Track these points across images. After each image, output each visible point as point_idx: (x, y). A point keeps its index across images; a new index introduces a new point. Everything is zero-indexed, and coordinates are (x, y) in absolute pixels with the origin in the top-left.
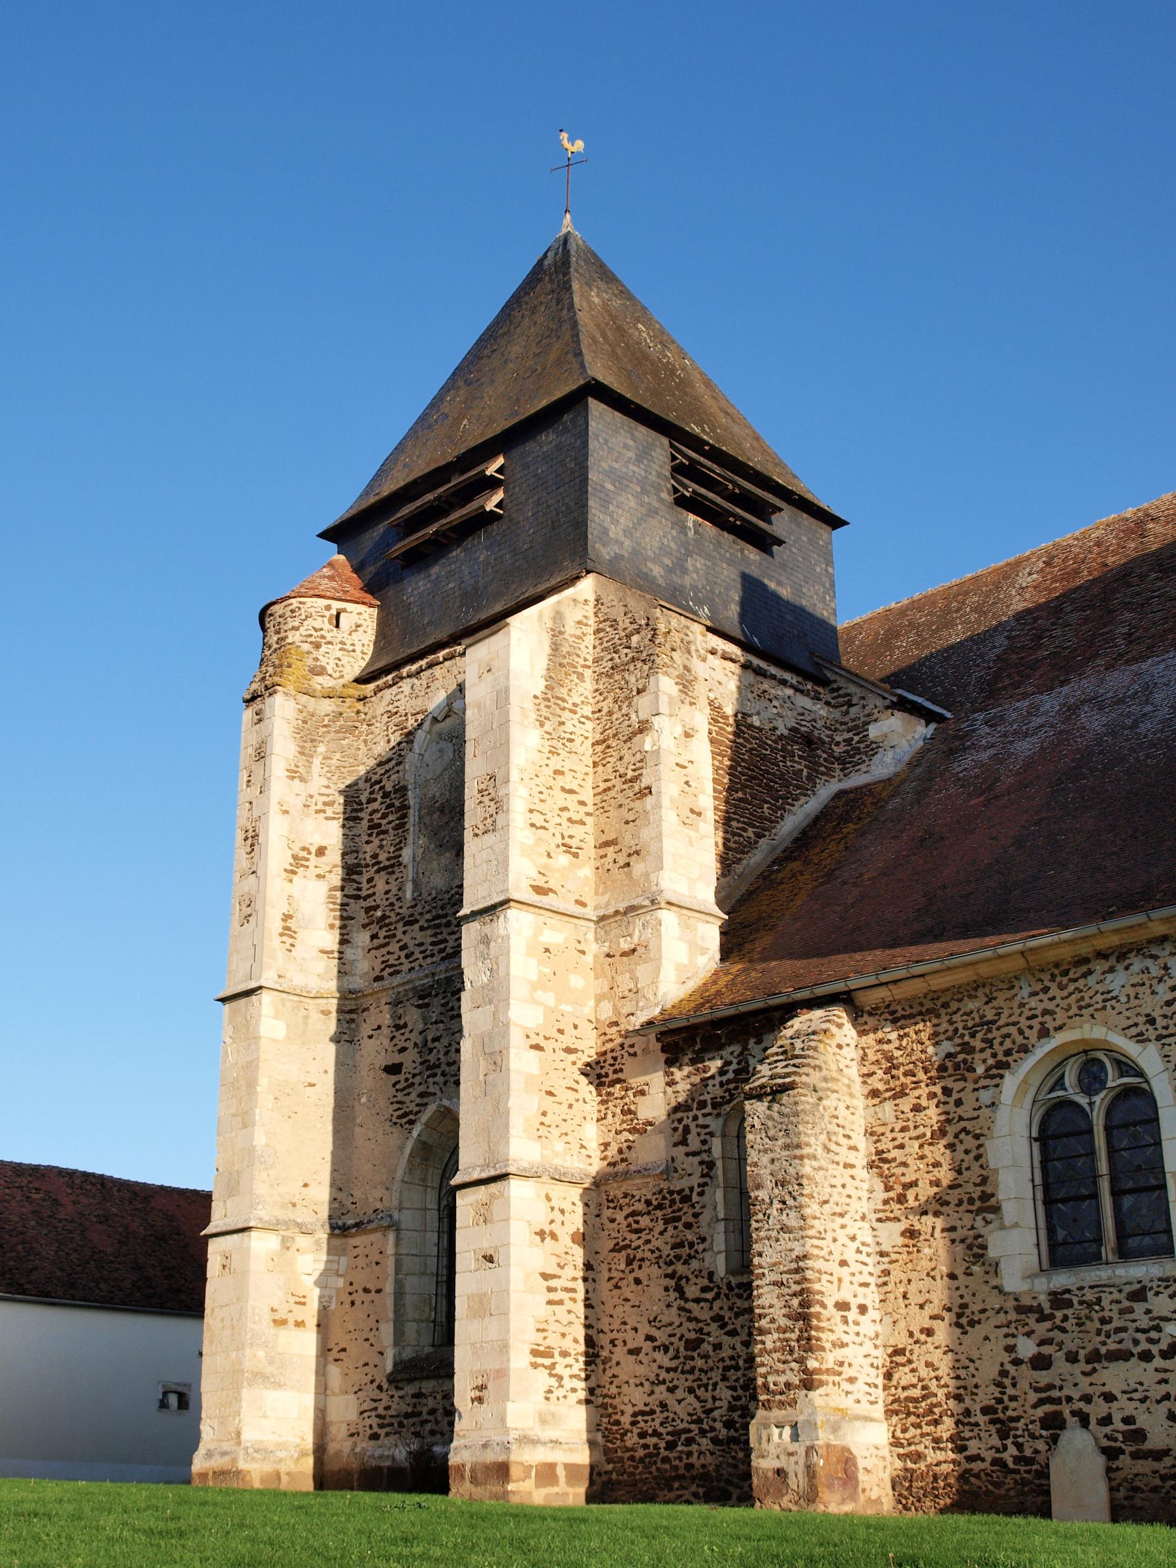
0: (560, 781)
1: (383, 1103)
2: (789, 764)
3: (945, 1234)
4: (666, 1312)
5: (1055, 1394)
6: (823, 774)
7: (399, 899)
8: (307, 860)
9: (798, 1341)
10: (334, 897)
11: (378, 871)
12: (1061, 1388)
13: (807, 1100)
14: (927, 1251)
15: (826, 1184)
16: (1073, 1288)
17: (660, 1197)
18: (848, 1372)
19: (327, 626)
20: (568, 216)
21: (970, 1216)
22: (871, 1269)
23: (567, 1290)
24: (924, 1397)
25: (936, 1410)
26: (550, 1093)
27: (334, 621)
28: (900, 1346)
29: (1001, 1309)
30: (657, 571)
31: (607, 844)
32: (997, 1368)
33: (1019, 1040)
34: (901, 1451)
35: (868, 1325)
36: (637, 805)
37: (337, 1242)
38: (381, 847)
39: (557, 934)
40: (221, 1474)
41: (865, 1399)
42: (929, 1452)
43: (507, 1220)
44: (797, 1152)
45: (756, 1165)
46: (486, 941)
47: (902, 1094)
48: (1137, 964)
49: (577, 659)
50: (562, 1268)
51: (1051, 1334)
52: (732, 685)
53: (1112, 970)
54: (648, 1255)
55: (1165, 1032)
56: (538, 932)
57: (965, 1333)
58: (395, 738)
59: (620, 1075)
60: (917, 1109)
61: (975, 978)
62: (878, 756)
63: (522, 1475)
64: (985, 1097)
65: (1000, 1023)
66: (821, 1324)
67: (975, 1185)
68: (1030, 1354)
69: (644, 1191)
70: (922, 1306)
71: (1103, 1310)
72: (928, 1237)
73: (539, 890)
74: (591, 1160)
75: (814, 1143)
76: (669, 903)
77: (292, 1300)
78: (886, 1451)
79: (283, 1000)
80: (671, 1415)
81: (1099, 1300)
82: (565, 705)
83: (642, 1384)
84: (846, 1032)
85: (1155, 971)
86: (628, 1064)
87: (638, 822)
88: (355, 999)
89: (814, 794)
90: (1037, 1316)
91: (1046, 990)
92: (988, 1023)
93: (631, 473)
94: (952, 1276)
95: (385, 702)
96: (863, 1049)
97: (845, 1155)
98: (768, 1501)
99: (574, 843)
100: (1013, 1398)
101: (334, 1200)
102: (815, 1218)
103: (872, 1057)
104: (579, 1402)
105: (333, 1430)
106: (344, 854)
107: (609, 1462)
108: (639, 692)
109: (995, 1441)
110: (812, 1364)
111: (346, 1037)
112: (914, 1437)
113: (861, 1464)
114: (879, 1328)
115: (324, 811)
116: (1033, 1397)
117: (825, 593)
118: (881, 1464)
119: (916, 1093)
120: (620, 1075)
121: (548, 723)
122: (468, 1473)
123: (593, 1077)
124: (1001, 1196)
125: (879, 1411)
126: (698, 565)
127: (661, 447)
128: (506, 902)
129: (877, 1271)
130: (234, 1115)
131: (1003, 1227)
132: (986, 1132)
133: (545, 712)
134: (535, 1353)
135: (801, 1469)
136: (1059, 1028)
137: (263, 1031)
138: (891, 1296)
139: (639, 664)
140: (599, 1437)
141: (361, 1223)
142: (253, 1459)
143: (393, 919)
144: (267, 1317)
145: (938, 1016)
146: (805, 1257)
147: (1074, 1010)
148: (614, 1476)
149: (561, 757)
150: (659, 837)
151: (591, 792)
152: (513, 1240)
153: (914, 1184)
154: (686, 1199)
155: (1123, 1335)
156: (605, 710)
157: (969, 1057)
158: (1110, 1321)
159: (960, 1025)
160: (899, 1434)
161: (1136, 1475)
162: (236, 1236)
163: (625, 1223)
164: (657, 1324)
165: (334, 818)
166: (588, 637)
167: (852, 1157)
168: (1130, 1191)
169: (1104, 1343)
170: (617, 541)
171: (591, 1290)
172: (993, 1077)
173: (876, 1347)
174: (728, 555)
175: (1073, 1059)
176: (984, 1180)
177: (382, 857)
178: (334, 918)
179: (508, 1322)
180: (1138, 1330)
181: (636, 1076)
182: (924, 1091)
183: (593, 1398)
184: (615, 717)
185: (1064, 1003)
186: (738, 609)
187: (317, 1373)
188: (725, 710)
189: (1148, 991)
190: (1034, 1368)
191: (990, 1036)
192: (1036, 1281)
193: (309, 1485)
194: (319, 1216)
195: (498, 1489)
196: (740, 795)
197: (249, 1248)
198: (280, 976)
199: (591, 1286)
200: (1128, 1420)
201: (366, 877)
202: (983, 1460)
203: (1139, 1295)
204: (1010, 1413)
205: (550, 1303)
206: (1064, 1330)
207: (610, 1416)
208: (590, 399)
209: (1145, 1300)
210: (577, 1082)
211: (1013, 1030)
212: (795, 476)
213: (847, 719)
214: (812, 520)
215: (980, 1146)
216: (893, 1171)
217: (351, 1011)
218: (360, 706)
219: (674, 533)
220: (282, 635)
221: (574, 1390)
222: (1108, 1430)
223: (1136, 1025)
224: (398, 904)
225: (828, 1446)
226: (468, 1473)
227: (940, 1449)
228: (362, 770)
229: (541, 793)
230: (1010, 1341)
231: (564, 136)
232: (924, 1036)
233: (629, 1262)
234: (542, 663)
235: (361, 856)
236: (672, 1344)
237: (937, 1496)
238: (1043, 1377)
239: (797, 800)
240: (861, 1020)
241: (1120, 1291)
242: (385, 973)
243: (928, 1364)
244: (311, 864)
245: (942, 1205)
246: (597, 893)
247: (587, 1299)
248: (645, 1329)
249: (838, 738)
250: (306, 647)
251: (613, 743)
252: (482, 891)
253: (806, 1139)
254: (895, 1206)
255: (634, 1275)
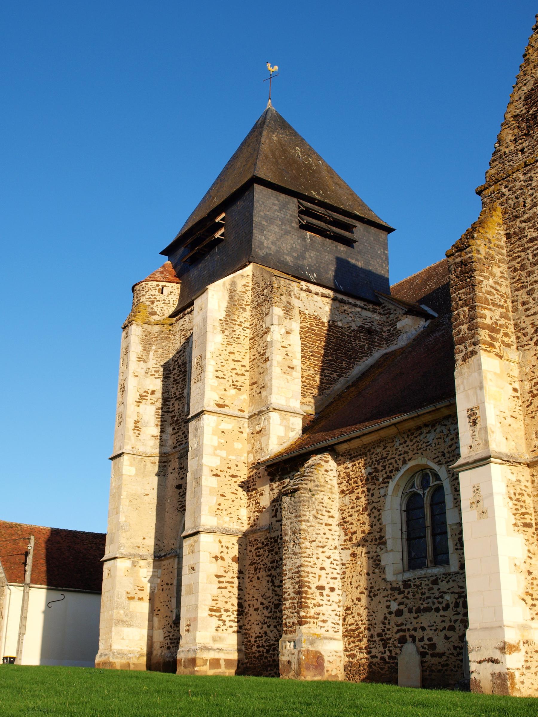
0: (232, 357)
1: (175, 502)
2: (357, 342)
3: (366, 555)
4: (268, 592)
5: (403, 627)
6: (376, 346)
7: (182, 412)
8: (147, 396)
9: (297, 603)
10: (158, 412)
11: (176, 400)
12: (406, 625)
13: (305, 495)
14: (359, 563)
15: (314, 533)
16: (412, 579)
17: (267, 540)
18: (321, 617)
19: (157, 293)
20: (270, 101)
21: (375, 546)
22: (338, 571)
23: (229, 582)
24: (357, 629)
25: (361, 635)
26: (223, 496)
27: (161, 291)
28: (349, 606)
29: (385, 588)
30: (289, 259)
31: (253, 384)
32: (383, 616)
33: (395, 465)
34: (348, 653)
35: (334, 597)
36: (264, 365)
37: (157, 563)
38: (177, 389)
39: (228, 425)
40: (105, 663)
41: (331, 630)
42: (358, 654)
43: (199, 552)
44: (300, 519)
45: (285, 525)
46: (196, 429)
47: (352, 492)
48: (439, 428)
49: (242, 302)
50: (227, 572)
51: (403, 600)
52: (327, 308)
53: (429, 432)
54: (262, 566)
55: (449, 460)
56: (218, 424)
57: (372, 600)
58: (183, 341)
59: (255, 487)
60: (358, 498)
61: (379, 438)
62: (401, 337)
63: (202, 664)
64: (382, 491)
65: (388, 458)
66: (308, 596)
67: (378, 532)
68: (395, 610)
69: (261, 538)
70: (357, 588)
71: (422, 589)
72: (360, 556)
73: (219, 406)
74: (243, 525)
75: (309, 515)
76: (274, 409)
77: (137, 588)
78: (342, 654)
79: (134, 458)
80: (268, 638)
81: (421, 584)
82: (236, 323)
83: (258, 624)
84: (332, 464)
85: (446, 432)
86: (258, 481)
87: (264, 373)
88: (166, 457)
89: (371, 355)
90: (398, 592)
91: (405, 442)
92: (384, 458)
93: (276, 216)
94: (368, 574)
95: (180, 326)
96: (339, 472)
97: (326, 519)
98: (284, 675)
99: (238, 384)
100: (388, 629)
101: (156, 545)
102: (307, 548)
103: (342, 475)
104: (234, 632)
105: (155, 645)
106: (163, 393)
107: (246, 658)
108: (266, 315)
109: (382, 649)
110: (302, 614)
111: (162, 473)
112: (352, 647)
113: (326, 659)
114: (341, 598)
115: (155, 375)
116: (396, 629)
117: (382, 263)
118: (339, 659)
119: (357, 491)
120: (255, 487)
121: (226, 331)
122: (183, 663)
123: (245, 488)
124: (387, 537)
125: (340, 635)
126: (312, 255)
127: (293, 204)
128: (202, 412)
129: (341, 572)
130: (114, 509)
131: (387, 552)
132: (382, 508)
133: (225, 326)
134: (211, 610)
135: (296, 661)
136: (410, 460)
137: (124, 472)
138: (346, 583)
139: (266, 302)
140: (243, 648)
141: (166, 554)
142: (117, 657)
143: (180, 421)
144: (125, 596)
145: (366, 456)
146: (301, 566)
147: (415, 451)
148: (248, 665)
149: (233, 346)
150: (271, 380)
151: (248, 361)
152: (201, 560)
153: (355, 532)
154: (276, 541)
155: (429, 600)
156: (254, 324)
157: (377, 474)
158: (425, 594)
159: (374, 460)
160: (347, 646)
161: (432, 664)
162: (112, 561)
163: (255, 553)
164: (265, 597)
165: (159, 378)
166: (249, 291)
167: (330, 521)
168: (439, 534)
169: (422, 604)
170: (268, 247)
171: (241, 582)
172: (385, 483)
173: (339, 606)
174: (328, 249)
175: (418, 474)
176: (381, 530)
177: (177, 394)
178: (158, 422)
179: (198, 596)
180: (435, 598)
181: (260, 487)
182: (360, 490)
183: (241, 630)
184: (258, 326)
185: (412, 448)
186: (333, 273)
187: (149, 620)
188: (323, 320)
189: (443, 441)
190: (396, 616)
191: (385, 464)
192: (398, 576)
193: (144, 668)
194: (150, 552)
195: (192, 670)
196: (330, 358)
197: (116, 566)
198: (133, 448)
199: (241, 581)
200: (430, 639)
201: (172, 402)
202: (377, 657)
203: (435, 582)
204: (387, 636)
205: (219, 588)
206: (408, 598)
207: (247, 638)
208: (255, 185)
209: (438, 584)
210: (237, 490)
211: (393, 461)
212: (370, 210)
213: (388, 320)
214: (376, 229)
215: (380, 515)
216: (348, 527)
217: (165, 462)
218: (170, 328)
219: (299, 241)
220: (139, 298)
221: (231, 627)
222: (422, 643)
223: (438, 457)
224: (182, 414)
225: (308, 651)
226: (183, 663)
227: (362, 653)
228: (171, 356)
229: (222, 362)
230: (388, 603)
231: (269, 65)
232: (361, 465)
233: (256, 570)
234: (224, 305)
235: (170, 394)
236: (269, 606)
237: (360, 674)
238: (400, 620)
239: (361, 358)
240: (338, 459)
241: (428, 580)
242: (177, 445)
243: (359, 614)
244: (148, 398)
245: (365, 542)
246: (249, 406)
247: (239, 586)
248: (260, 599)
249: (385, 329)
250: (148, 303)
251: (257, 338)
252: (196, 408)
253: (304, 513)
254: (348, 543)
255: (257, 575)
